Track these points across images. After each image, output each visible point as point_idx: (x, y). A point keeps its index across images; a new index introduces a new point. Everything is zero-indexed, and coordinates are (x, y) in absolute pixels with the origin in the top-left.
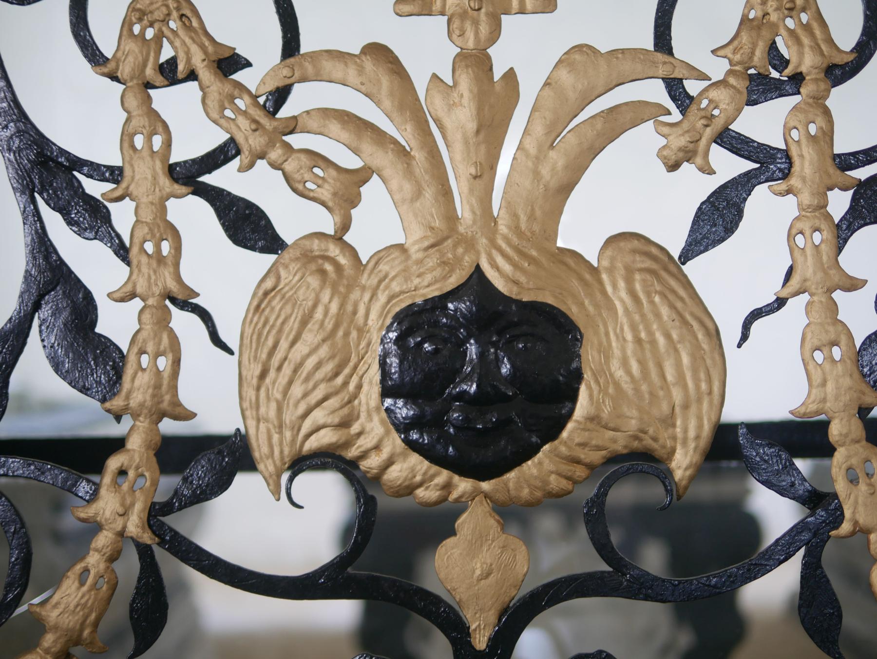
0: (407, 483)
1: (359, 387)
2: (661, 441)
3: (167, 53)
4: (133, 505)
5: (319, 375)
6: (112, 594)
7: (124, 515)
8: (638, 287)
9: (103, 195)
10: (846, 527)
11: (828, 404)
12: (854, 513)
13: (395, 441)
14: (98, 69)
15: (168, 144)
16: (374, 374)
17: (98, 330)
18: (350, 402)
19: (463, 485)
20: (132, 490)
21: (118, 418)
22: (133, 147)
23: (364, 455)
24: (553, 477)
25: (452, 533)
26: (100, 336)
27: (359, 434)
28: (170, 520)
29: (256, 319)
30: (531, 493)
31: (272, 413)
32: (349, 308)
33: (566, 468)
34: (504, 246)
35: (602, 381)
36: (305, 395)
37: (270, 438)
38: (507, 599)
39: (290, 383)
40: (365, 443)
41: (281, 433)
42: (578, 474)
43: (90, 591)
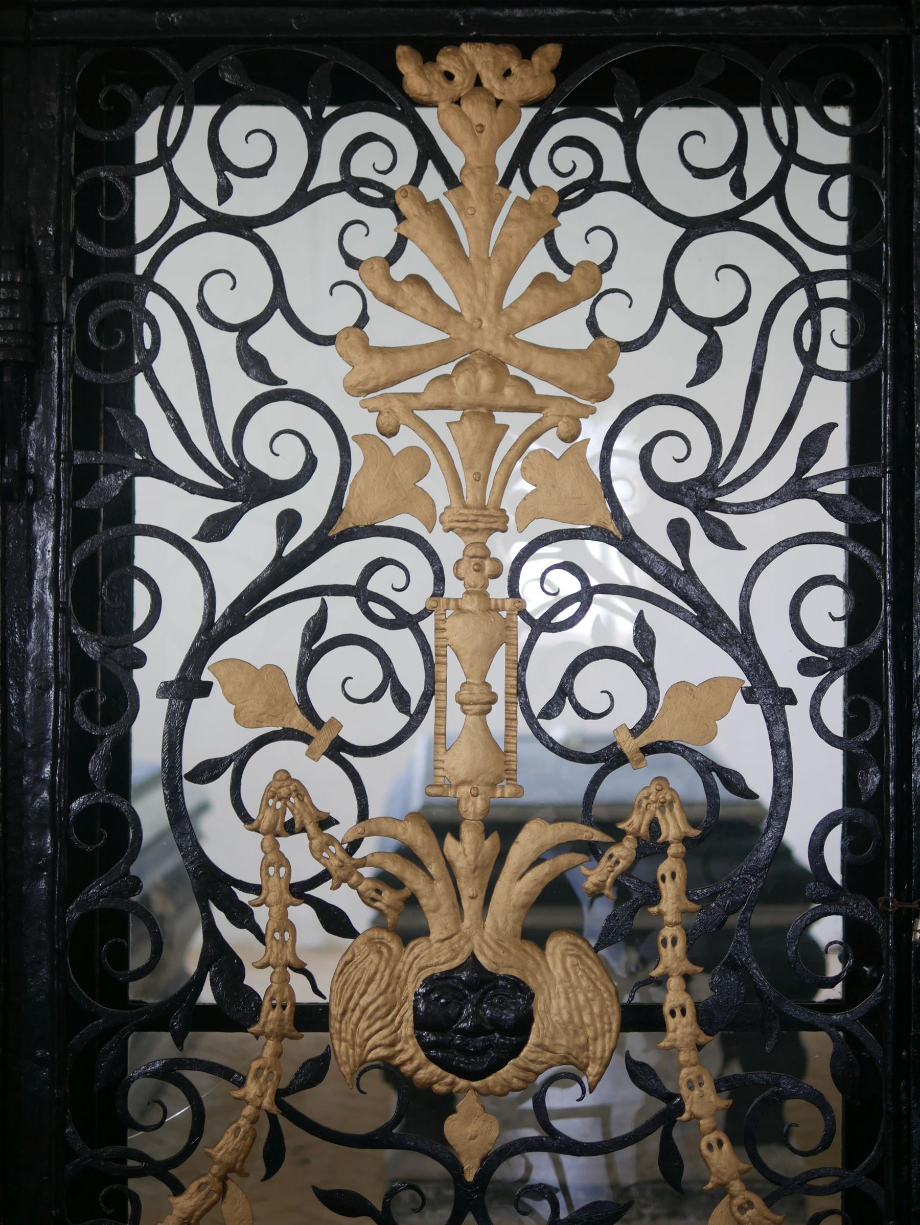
0: (428, 1081)
1: (401, 1023)
2: (580, 1059)
3: (289, 816)
4: (266, 1090)
5: (379, 1014)
6: (253, 1143)
7: (262, 1096)
8: (568, 965)
9: (249, 902)
10: (685, 1116)
11: (678, 1042)
12: (691, 1107)
13: (421, 1055)
14: (248, 826)
15: (289, 873)
16: (410, 1015)
17: (245, 982)
18: (395, 1031)
19: (462, 1083)
20: (266, 1081)
21: (257, 1037)
22: (268, 874)
23: (403, 1063)
24: (515, 1080)
25: (454, 1111)
26: (247, 986)
27: (401, 1051)
28: (287, 1099)
29: (340, 979)
30: (502, 1089)
31: (349, 1037)
32: (396, 973)
33: (522, 1074)
34: (488, 940)
35: (545, 1023)
36: (369, 1027)
37: (347, 1052)
38: (486, 1152)
39: (359, 1019)
40: (403, 1057)
41: (354, 1049)
42: (530, 1078)
43: (240, 1141)
